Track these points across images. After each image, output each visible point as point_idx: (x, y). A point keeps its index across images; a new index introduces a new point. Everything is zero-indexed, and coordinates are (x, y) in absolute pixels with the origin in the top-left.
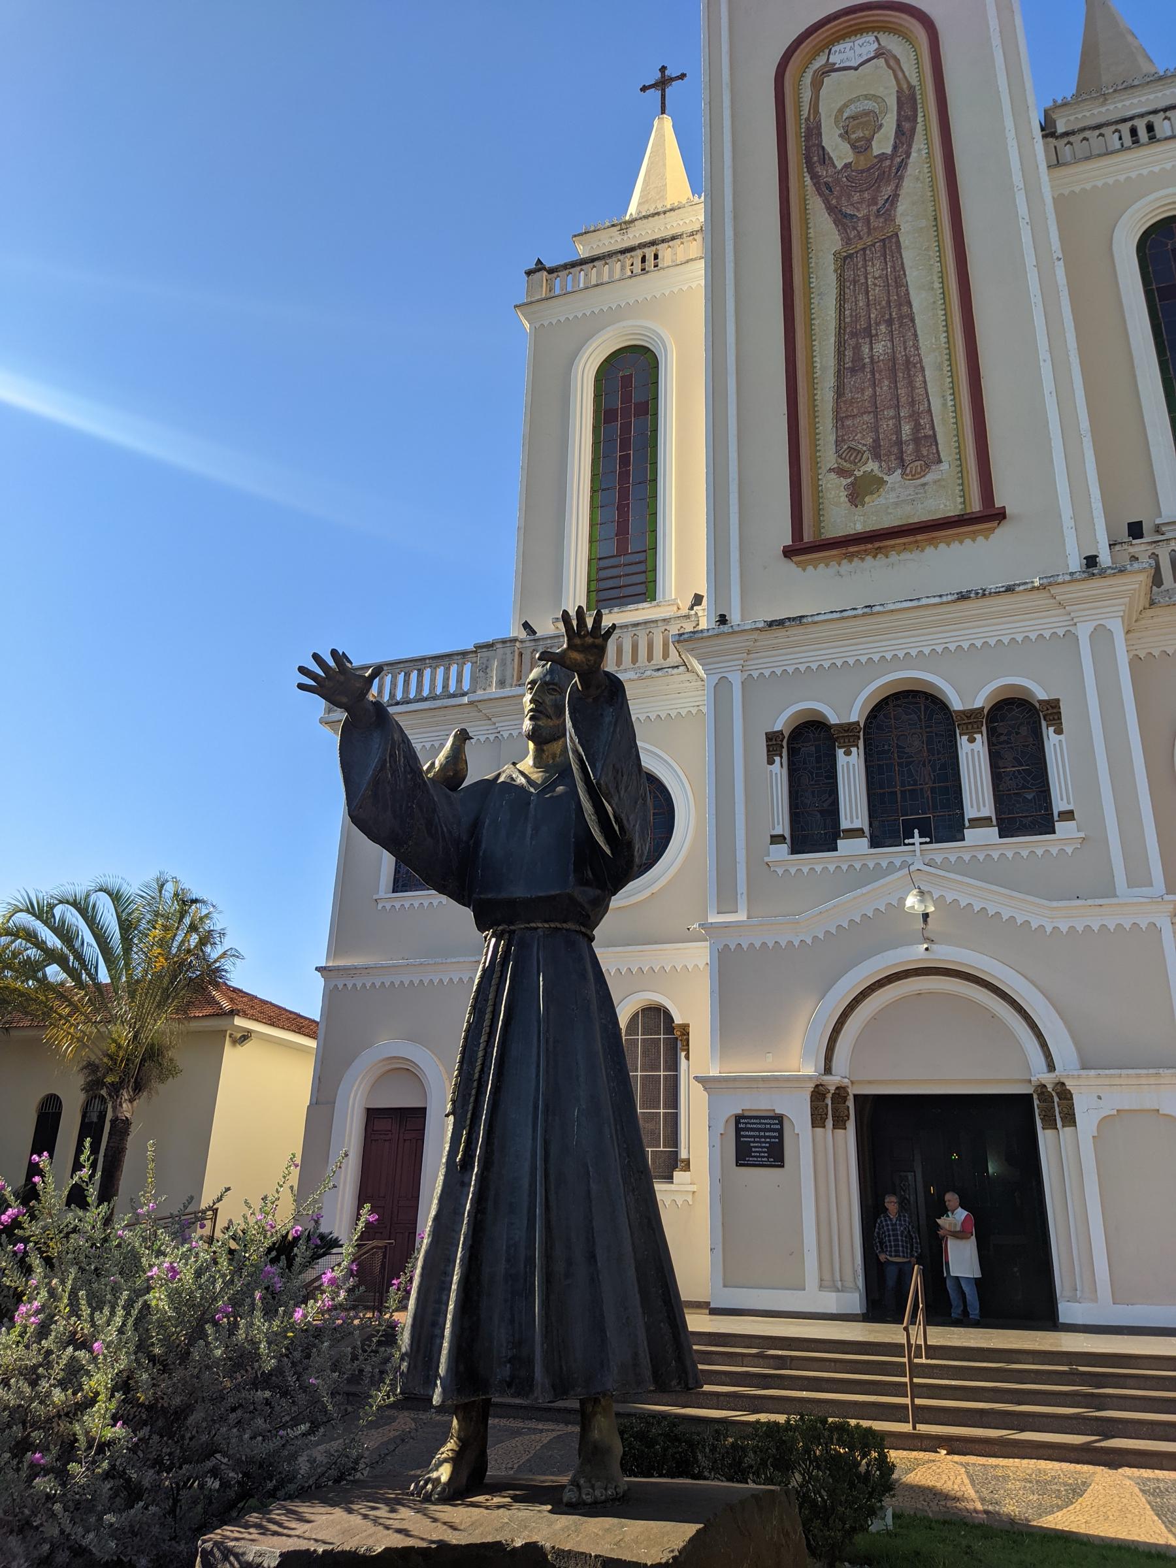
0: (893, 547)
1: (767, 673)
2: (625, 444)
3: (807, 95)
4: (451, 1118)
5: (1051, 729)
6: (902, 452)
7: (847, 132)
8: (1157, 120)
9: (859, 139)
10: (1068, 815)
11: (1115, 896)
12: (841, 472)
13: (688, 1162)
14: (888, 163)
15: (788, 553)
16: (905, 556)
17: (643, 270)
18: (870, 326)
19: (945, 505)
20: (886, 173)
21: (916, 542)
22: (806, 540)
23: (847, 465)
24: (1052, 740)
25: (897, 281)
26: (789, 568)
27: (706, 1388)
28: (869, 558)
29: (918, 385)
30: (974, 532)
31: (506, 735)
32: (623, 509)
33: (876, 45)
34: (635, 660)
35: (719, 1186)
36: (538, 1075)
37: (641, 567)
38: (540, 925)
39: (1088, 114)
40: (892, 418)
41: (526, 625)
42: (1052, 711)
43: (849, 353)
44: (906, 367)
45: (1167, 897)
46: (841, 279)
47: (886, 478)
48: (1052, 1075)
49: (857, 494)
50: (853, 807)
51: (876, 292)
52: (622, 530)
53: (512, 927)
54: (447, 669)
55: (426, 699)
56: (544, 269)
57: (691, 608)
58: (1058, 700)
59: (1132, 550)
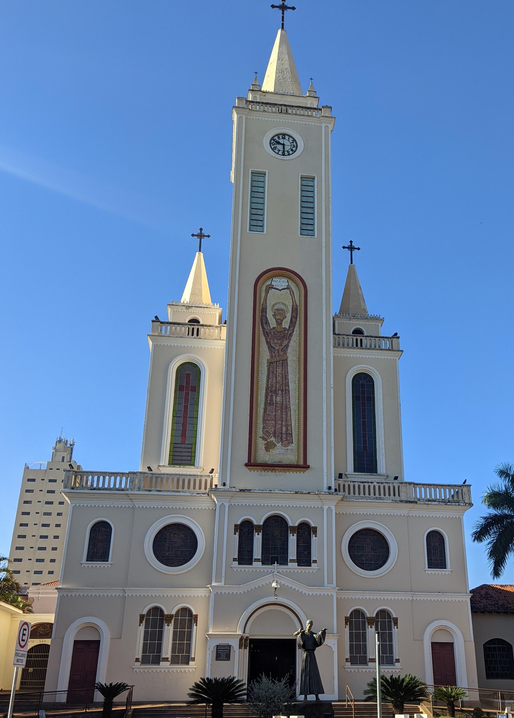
1: (236, 504)
3: (263, 294)
9: (279, 319)
10: (315, 562)
11: (324, 586)
12: (264, 439)
13: (194, 658)
14: (287, 332)
15: (246, 465)
16: (281, 473)
20: (285, 335)
24: (314, 539)
25: (285, 377)
26: (246, 469)
28: (270, 471)
31: (137, 506)
32: (184, 425)
34: (189, 488)
41: (149, 468)
42: (315, 530)
44: (285, 408)
46: (268, 369)
49: (269, 447)
50: (257, 553)
51: (279, 378)
52: (184, 435)
54: (115, 479)
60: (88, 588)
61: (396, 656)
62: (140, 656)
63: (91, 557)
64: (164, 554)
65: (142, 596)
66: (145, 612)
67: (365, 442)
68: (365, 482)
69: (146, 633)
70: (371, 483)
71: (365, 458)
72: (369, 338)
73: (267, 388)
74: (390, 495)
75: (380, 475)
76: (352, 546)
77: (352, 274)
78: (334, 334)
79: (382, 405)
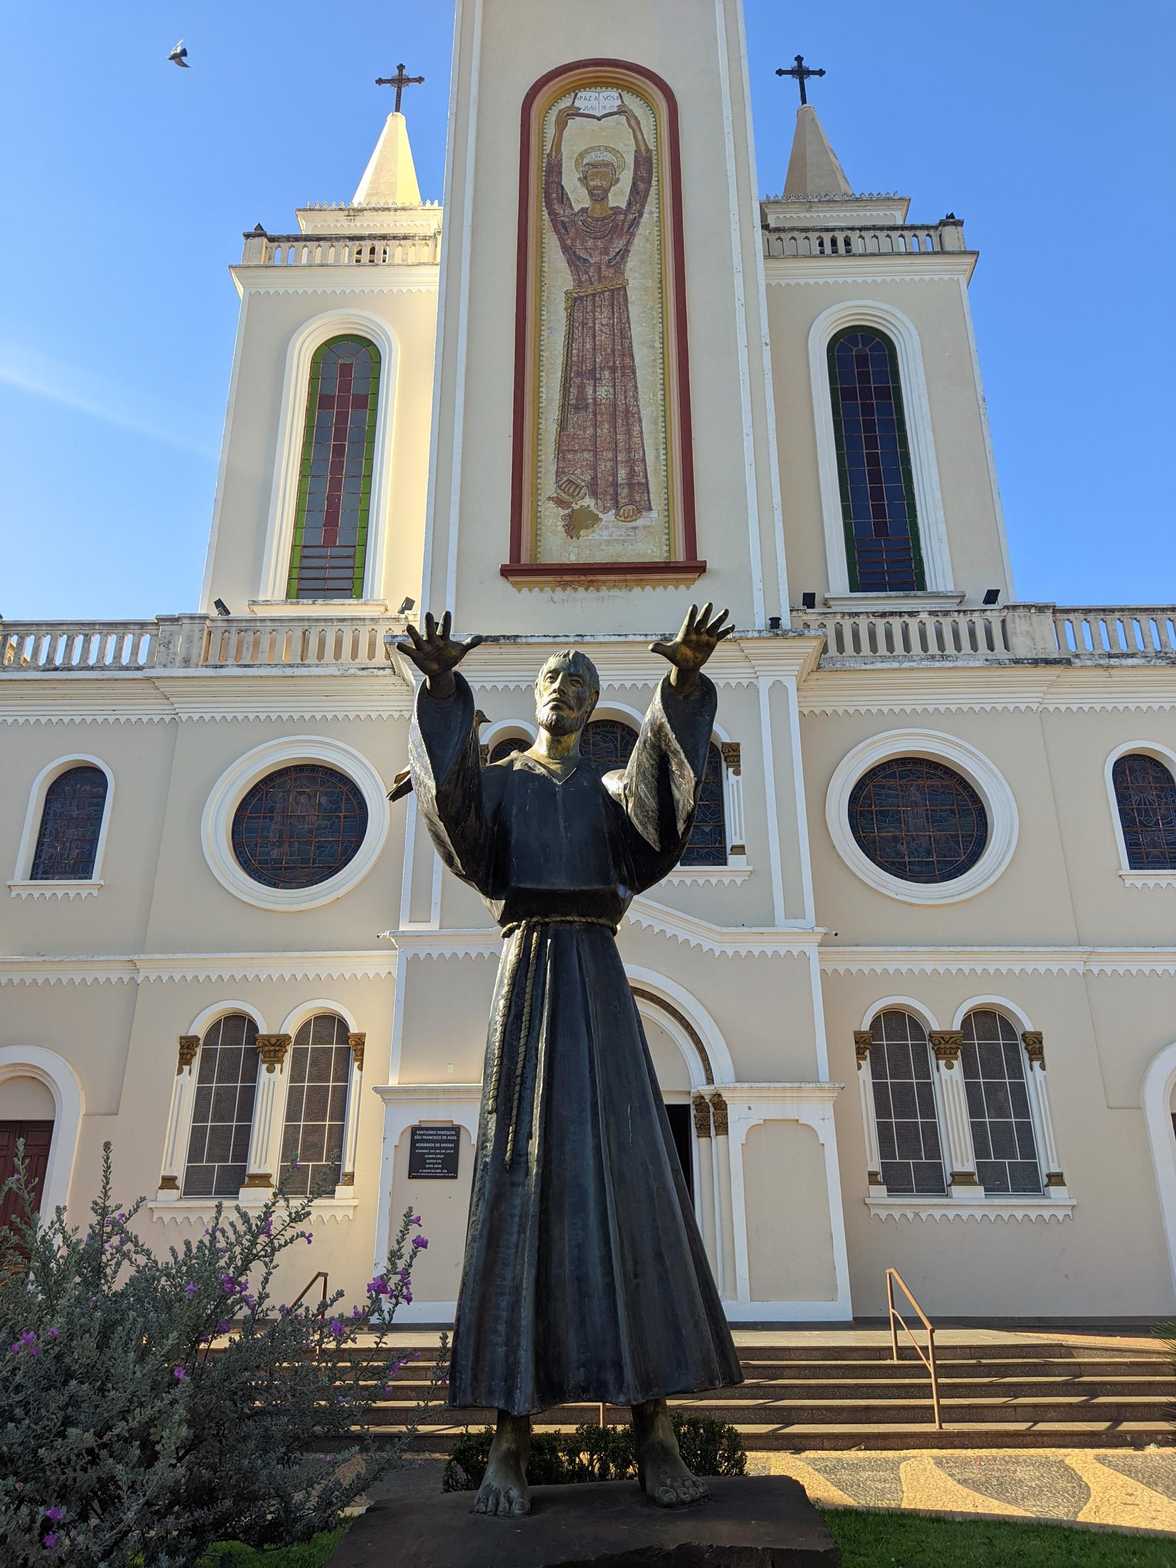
0: (604, 582)
2: (340, 434)
4: (494, 1116)
5: (731, 770)
6: (617, 494)
7: (586, 178)
8: (854, 236)
10: (739, 850)
12: (560, 502)
13: (352, 1175)
14: (622, 217)
15: (505, 572)
16: (615, 592)
17: (358, 261)
18: (595, 369)
19: (650, 550)
20: (621, 226)
21: (625, 581)
22: (523, 562)
23: (565, 497)
25: (622, 332)
26: (504, 585)
27: (747, 1382)
28: (581, 589)
29: (635, 433)
30: (677, 580)
31: (184, 717)
33: (619, 102)
34: (338, 655)
35: (389, 1199)
36: (592, 1069)
37: (348, 562)
38: (576, 919)
39: (795, 216)
40: (610, 460)
41: (219, 604)
43: (574, 391)
44: (624, 415)
45: (817, 929)
46: (570, 317)
47: (601, 515)
48: (711, 1087)
49: (575, 524)
51: (603, 338)
52: (332, 520)
53: (547, 920)
54: (121, 640)
55: (92, 668)
56: (264, 235)
57: (402, 612)
58: (738, 744)
59: (805, 617)
60: (23, 958)
61: (1047, 1164)
62: (179, 1169)
63: (43, 868)
64: (268, 854)
65: (189, 978)
66: (199, 1029)
67: (879, 511)
68: (892, 614)
69: (202, 1096)
70: (911, 614)
71: (884, 549)
72: (872, 233)
73: (567, 367)
74: (975, 648)
75: (936, 596)
76: (862, 813)
77: (805, 128)
78: (765, 227)
79: (925, 403)
